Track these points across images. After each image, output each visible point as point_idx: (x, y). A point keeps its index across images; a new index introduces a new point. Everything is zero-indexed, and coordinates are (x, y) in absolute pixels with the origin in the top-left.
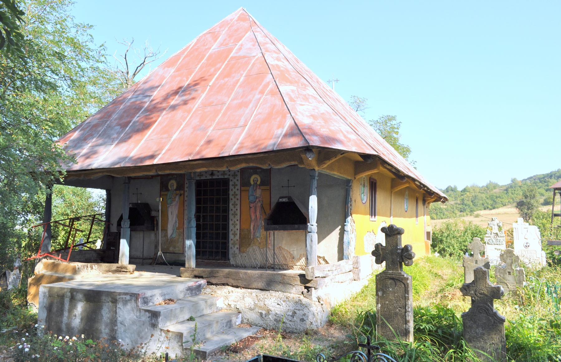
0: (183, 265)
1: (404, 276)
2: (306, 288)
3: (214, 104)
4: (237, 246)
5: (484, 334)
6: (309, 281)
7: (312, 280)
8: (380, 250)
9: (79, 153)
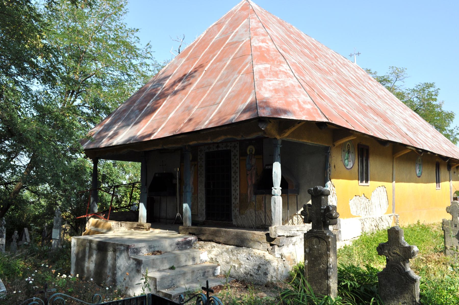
0: (182, 224)
1: (326, 234)
2: (272, 245)
3: (204, 86)
4: (238, 209)
5: (397, 293)
6: (273, 239)
7: (275, 238)
8: (307, 210)
9: (107, 134)
